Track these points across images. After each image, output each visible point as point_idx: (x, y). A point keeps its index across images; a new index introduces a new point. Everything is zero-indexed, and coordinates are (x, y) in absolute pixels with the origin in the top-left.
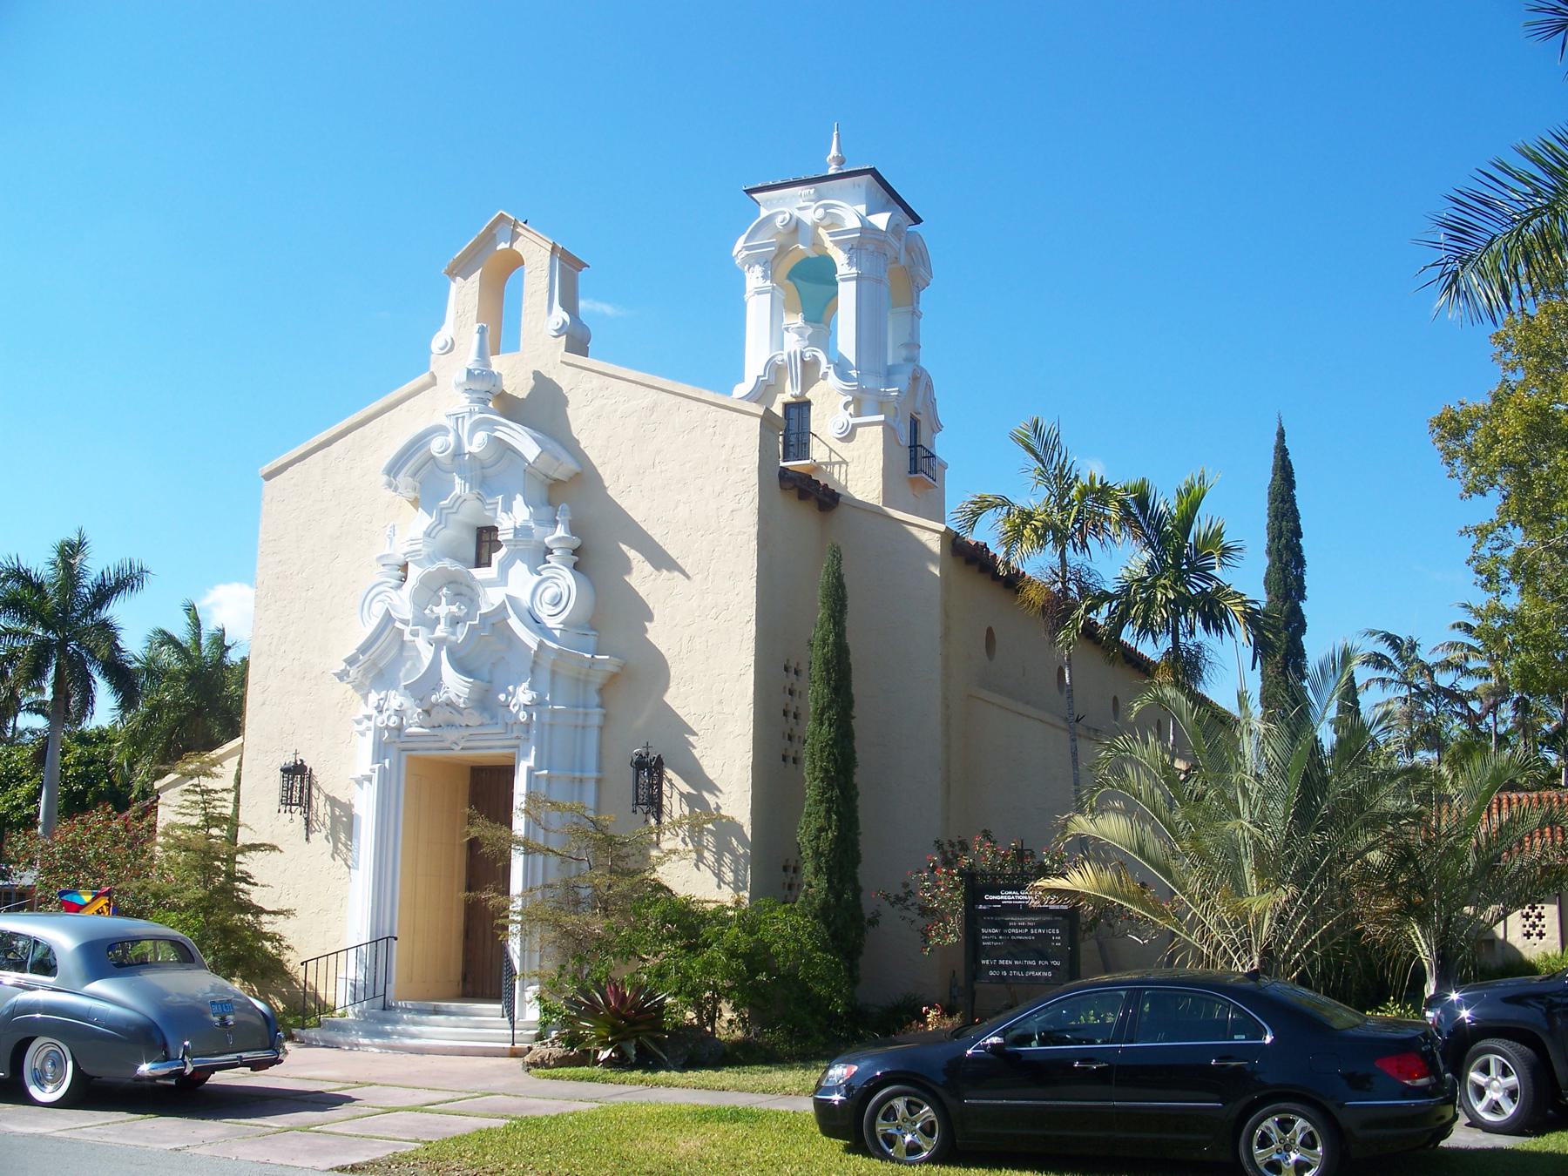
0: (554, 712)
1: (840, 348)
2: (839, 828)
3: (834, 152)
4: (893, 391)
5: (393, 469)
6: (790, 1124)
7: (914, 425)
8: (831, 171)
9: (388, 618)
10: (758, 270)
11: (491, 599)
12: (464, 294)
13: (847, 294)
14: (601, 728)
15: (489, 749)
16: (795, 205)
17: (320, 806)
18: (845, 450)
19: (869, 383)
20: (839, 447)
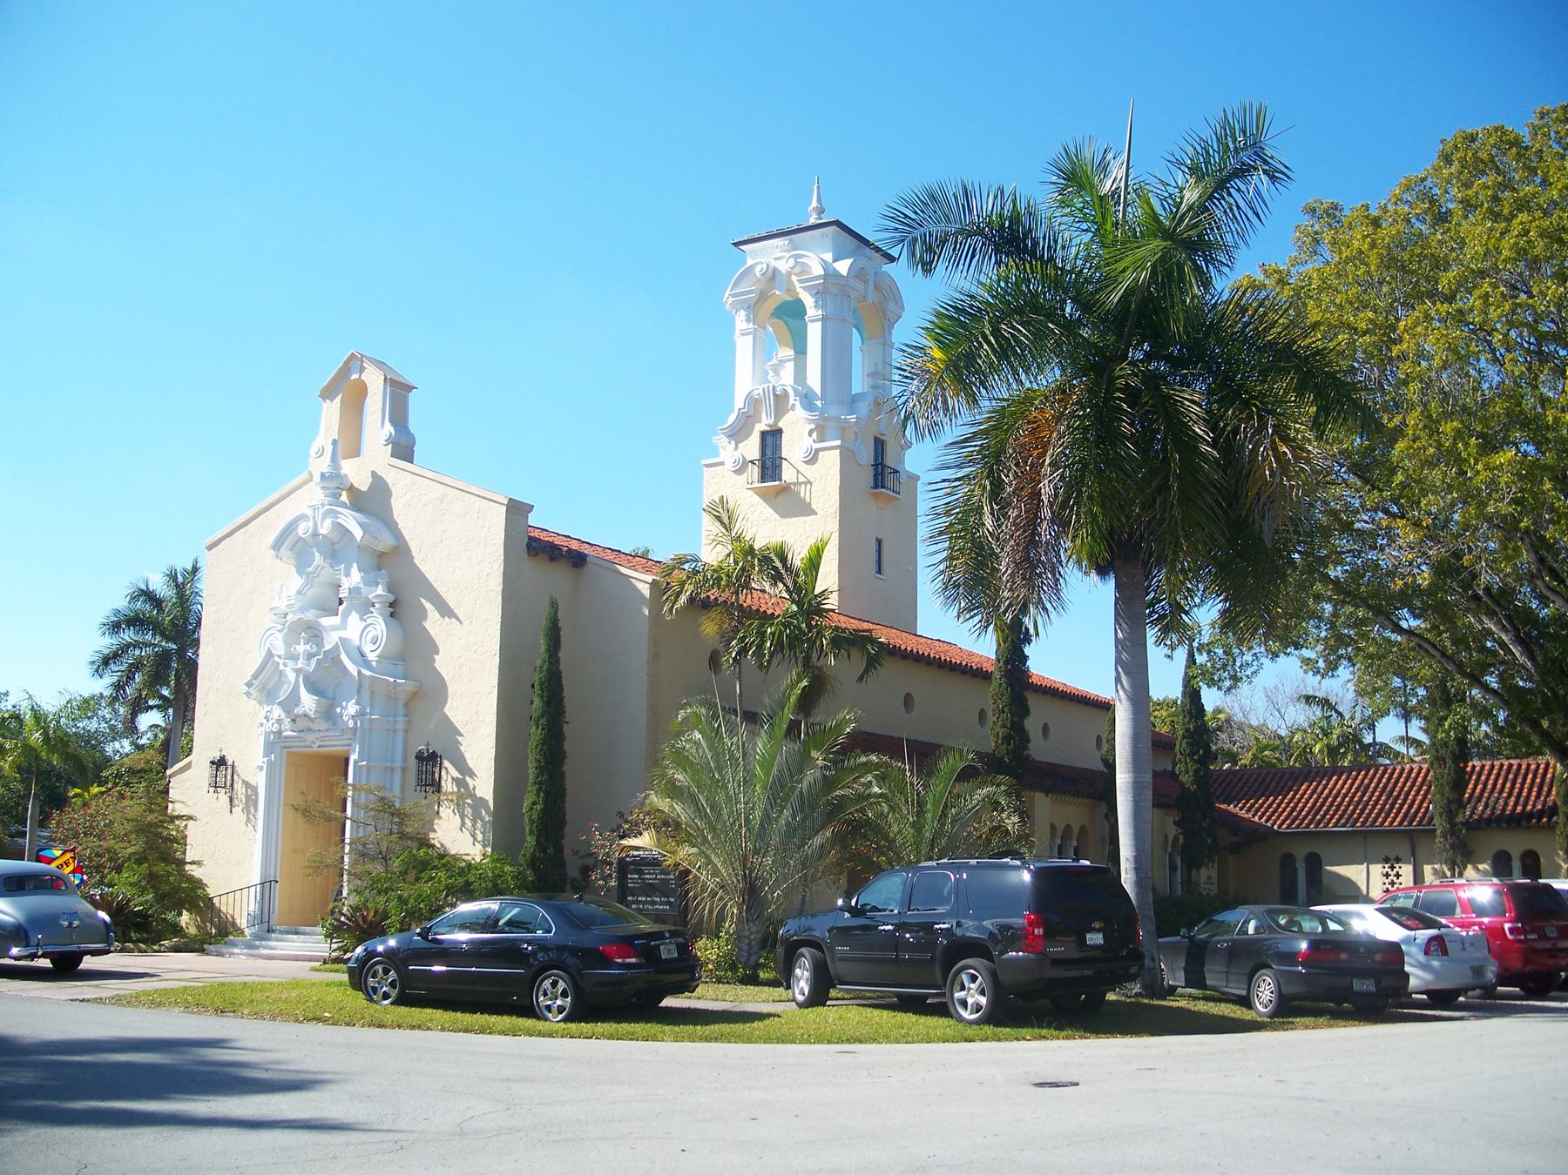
0: (371, 720)
1: (809, 382)
2: (545, 803)
4: (852, 418)
5: (277, 545)
6: (341, 984)
7: (879, 445)
8: (813, 220)
9: (270, 655)
10: (743, 313)
11: (331, 640)
12: (331, 412)
13: (814, 332)
14: (406, 731)
15: (335, 746)
16: (774, 255)
17: (239, 787)
18: (810, 472)
19: (833, 411)
20: (804, 468)
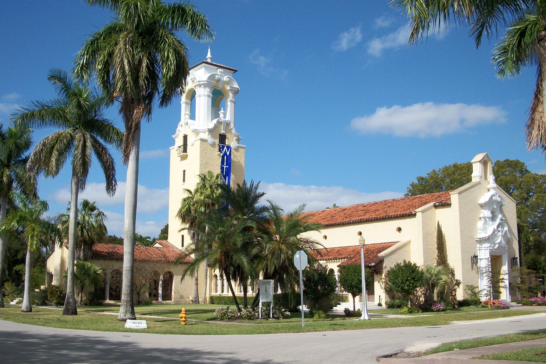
3: (209, 55)
